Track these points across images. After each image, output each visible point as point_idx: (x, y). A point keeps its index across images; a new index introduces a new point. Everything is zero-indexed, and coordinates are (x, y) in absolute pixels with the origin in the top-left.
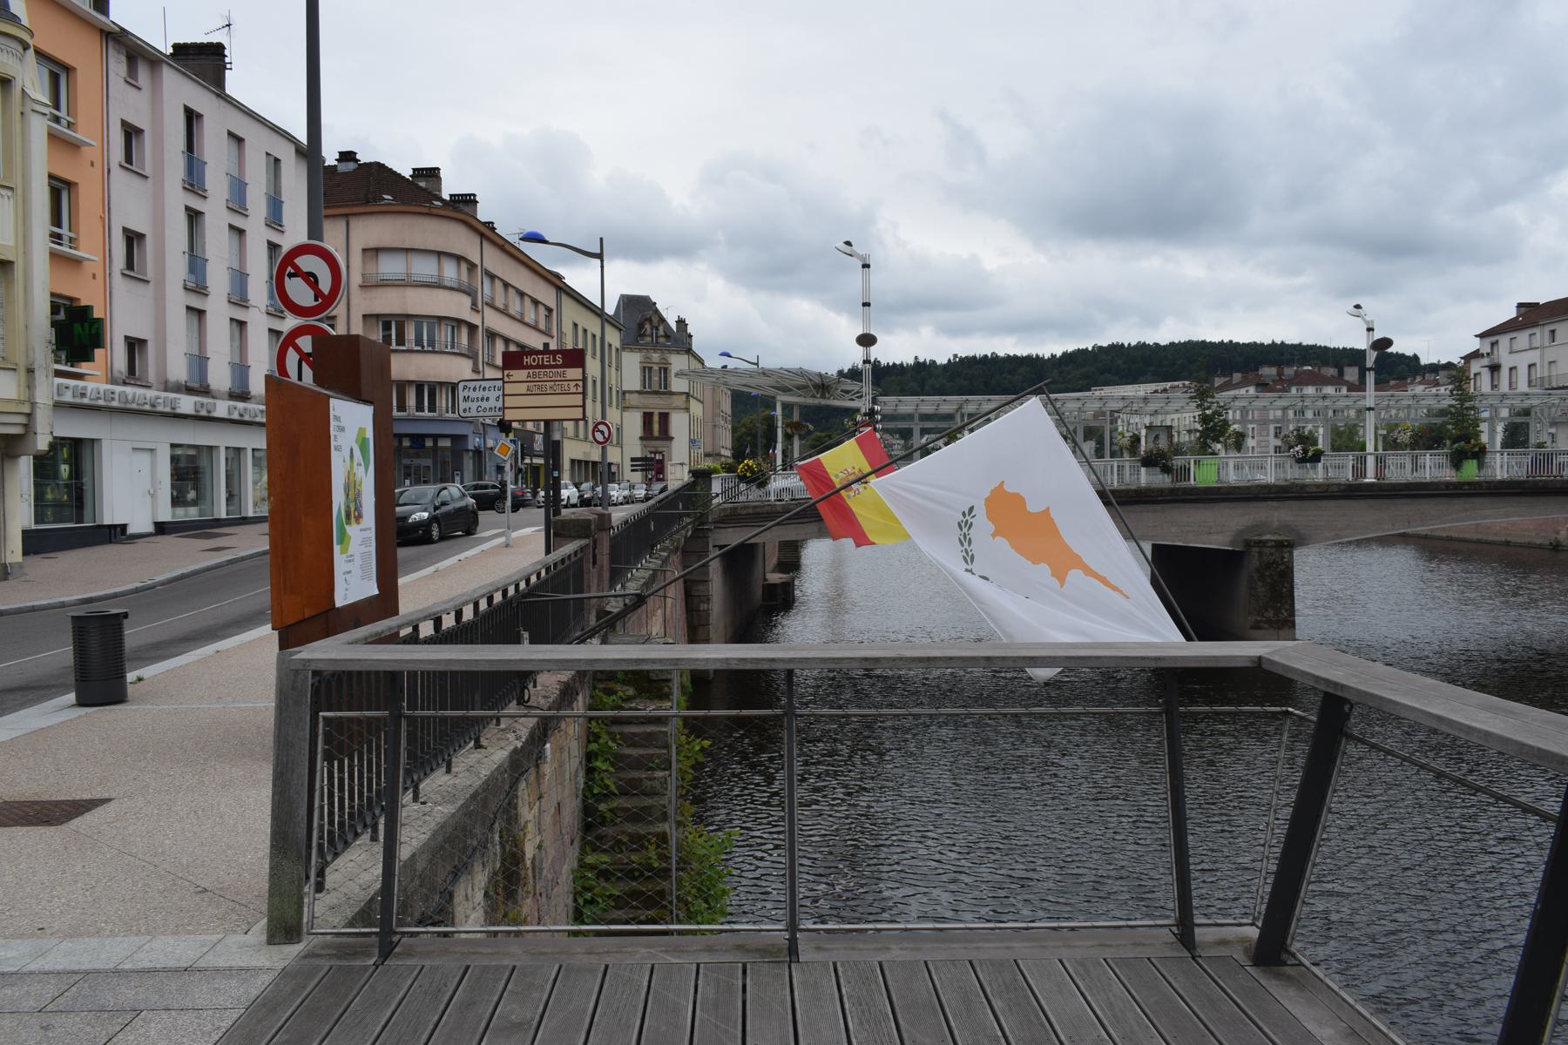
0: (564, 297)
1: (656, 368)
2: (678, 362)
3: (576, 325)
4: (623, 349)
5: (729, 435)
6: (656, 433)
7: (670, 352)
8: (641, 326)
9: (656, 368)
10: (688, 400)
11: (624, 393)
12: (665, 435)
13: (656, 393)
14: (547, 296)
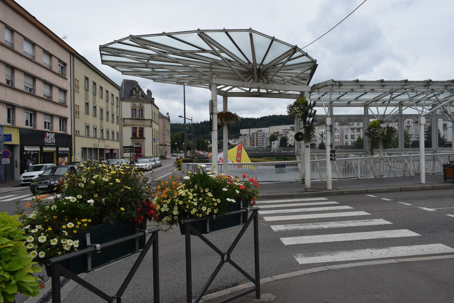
0: (76, 60)
1: (138, 109)
2: (147, 108)
3: (87, 79)
4: (122, 100)
5: (169, 138)
6: (138, 136)
7: (144, 102)
8: (132, 92)
9: (138, 109)
10: (151, 123)
11: (124, 119)
12: (142, 136)
13: (138, 119)
14: (66, 57)
